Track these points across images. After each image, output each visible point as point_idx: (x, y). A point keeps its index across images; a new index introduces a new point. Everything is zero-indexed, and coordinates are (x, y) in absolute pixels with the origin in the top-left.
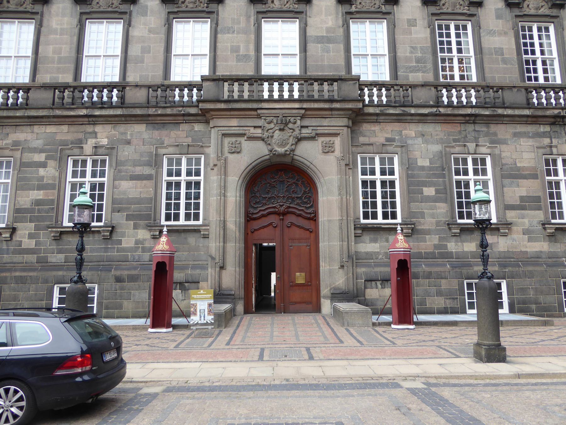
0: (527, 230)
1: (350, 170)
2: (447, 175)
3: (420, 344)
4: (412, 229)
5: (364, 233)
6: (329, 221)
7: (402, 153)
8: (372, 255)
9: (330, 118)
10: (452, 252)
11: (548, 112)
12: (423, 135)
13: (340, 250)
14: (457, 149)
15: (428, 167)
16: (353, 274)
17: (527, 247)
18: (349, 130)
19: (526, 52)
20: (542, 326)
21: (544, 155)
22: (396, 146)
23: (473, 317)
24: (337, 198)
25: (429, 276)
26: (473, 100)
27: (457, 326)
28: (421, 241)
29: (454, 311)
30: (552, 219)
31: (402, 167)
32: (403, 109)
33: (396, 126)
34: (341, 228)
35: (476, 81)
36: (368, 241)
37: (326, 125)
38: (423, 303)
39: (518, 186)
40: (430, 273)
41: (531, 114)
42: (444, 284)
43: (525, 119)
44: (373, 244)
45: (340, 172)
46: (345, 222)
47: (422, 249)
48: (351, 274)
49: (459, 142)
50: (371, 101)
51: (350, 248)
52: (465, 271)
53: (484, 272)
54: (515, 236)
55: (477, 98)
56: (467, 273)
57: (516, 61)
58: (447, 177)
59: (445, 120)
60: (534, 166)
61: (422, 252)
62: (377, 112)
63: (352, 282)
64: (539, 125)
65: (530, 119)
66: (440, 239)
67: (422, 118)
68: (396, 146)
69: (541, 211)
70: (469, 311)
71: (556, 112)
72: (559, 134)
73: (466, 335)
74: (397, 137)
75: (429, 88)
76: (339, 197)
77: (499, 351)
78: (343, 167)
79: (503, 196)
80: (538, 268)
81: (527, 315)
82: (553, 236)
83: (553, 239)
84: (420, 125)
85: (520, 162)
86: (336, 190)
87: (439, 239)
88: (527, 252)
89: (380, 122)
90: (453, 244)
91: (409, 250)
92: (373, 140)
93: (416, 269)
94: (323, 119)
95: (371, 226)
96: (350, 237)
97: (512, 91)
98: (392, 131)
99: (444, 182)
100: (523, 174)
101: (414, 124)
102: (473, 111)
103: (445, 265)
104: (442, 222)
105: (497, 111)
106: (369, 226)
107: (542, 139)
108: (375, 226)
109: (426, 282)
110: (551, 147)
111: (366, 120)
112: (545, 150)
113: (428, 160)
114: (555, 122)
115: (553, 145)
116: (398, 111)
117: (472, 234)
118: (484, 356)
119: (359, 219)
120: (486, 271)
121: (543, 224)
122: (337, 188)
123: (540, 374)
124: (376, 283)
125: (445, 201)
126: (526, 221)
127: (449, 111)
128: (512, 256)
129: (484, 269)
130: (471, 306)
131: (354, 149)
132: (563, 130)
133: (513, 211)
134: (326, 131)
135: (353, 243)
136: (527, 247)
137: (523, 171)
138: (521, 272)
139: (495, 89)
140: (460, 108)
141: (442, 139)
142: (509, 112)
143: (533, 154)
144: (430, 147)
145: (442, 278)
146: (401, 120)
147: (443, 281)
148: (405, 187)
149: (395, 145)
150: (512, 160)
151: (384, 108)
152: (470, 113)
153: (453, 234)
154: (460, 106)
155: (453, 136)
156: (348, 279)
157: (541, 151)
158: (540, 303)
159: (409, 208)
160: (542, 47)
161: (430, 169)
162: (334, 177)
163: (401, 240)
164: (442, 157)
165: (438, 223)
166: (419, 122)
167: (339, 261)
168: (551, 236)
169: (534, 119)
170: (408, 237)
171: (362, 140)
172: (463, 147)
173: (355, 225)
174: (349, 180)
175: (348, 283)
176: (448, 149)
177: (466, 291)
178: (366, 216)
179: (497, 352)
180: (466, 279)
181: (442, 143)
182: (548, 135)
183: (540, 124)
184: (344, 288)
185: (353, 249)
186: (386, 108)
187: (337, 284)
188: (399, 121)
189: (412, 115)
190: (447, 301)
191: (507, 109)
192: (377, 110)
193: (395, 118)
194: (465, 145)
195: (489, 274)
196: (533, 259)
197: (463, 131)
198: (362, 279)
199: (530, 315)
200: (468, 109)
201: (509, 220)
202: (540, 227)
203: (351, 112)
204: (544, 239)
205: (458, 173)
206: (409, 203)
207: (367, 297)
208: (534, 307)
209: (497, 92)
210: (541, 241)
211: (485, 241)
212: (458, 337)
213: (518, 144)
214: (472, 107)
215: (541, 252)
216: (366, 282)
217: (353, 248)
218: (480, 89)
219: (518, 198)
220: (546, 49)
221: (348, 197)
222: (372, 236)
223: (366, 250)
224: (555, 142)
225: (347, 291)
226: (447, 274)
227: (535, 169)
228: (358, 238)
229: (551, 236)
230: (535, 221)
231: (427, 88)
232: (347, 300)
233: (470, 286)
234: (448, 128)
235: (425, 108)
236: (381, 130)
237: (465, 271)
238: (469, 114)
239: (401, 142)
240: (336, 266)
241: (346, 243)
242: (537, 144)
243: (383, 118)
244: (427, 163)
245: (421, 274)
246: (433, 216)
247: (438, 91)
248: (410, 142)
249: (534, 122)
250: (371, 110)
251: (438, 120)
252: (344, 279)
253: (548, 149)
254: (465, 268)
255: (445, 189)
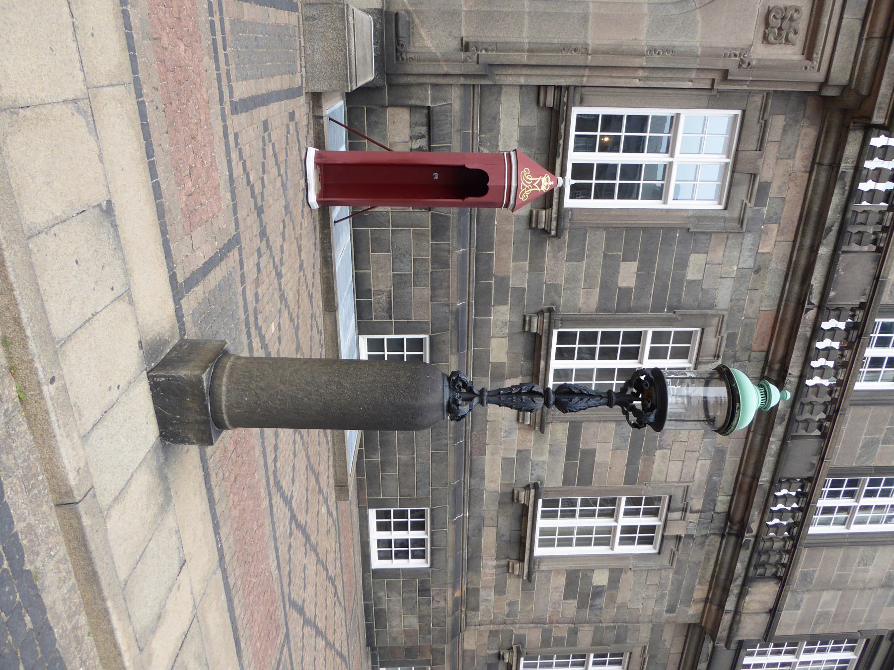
0: (528, 458)
1: (709, 82)
2: (658, 315)
3: (244, 193)
4: (546, 232)
5: (545, 114)
6: (585, 19)
7: (725, 220)
8: (491, 131)
9: (861, 34)
10: (489, 313)
11: (756, 513)
12: (757, 271)
13: (507, 43)
14: (711, 341)
15: (684, 275)
16: (446, 75)
17: (493, 454)
18: (813, 88)
19: (873, 483)
20: (336, 480)
21: (670, 497)
22: (744, 208)
23: (351, 348)
24: (644, 43)
25: (440, 260)
26: (815, 380)
27: (325, 310)
28: (516, 249)
29: (362, 310)
30: (544, 501)
31: (693, 217)
32: (835, 228)
33: (791, 212)
34: (564, 48)
35: (855, 388)
36: (525, 122)
37: (844, 21)
38: (379, 244)
39: (615, 449)
40: (446, 265)
41: (760, 483)
42: (421, 293)
43: (750, 471)
44: (516, 135)
45: (711, 53)
46: (579, 60)
47: (498, 251)
48: (445, 69)
49: (727, 346)
50: (873, 153)
51: (511, 71)
52: (448, 337)
53: (470, 390)
54: (516, 436)
55: (815, 389)
56: (444, 342)
57: (864, 465)
58: (654, 315)
59: (782, 321)
60: (652, 478)
61: (492, 249)
62: (843, 165)
63: (426, 72)
64: (731, 493)
65: (748, 480)
66: (519, 291)
67: (800, 272)
68: (744, 208)
69: (561, 484)
70: (363, 340)
71: (754, 526)
72: (705, 526)
73: (297, 329)
74: (765, 210)
75: (867, 292)
76: (646, 49)
77: (197, 422)
78: (721, 65)
79: (600, 422)
80: (451, 471)
81: (361, 446)
82: (513, 500)
83: (507, 499)
84: (783, 267)
85: (663, 457)
86: (661, 40)
87: (519, 289)
88: (484, 454)
89: (810, 173)
90: (508, 317)
91: (512, 202)
92: (771, 150)
93: (455, 235)
94: (863, 12)
95: (562, 131)
96: (538, 72)
97: (815, 455)
98: (783, 199)
99: (645, 309)
100: (638, 459)
101: (788, 253)
102: (792, 379)
103: (461, 299)
104: (556, 298)
105: (780, 424)
106: (563, 126)
107: (702, 496)
108: (561, 142)
109: (425, 253)
110: (684, 510)
111: (826, 137)
112: (680, 500)
113: (698, 277)
114: (731, 522)
115: (688, 514)
116: (833, 215)
117: (525, 356)
118: (173, 373)
119: (581, 103)
120: (476, 400)
121: (536, 486)
122: (668, 43)
123: (95, 574)
124: (423, 137)
125: (601, 308)
126: (545, 457)
127: (804, 330)
128: (477, 427)
129: (482, 391)
130: (375, 345)
131: (758, 100)
132: (712, 532)
133: (566, 437)
134: (825, 21)
135: (522, 81)
136: (493, 454)
137: (644, 460)
138: (445, 442)
139: (827, 424)
140: (804, 354)
141: (741, 310)
142: (774, 446)
143: (676, 480)
144: (729, 283)
145: (433, 289)
146: (806, 224)
147: (427, 292)
148: (643, 222)
149: (749, 205)
150: (670, 441)
151: (848, 184)
152: (790, 371)
153: (527, 319)
154: (810, 353)
155: (743, 335)
156: (434, 60)
157: (679, 494)
158: (383, 471)
159: (596, 228)
160: (875, 509)
161: (679, 281)
162: (698, 37)
163: (540, 185)
164: (699, 307)
165: (554, 288)
166: (791, 265)
167: (480, 40)
168: (513, 497)
169: (746, 487)
170: (527, 221)
171: (778, 122)
172: (713, 353)
173: (568, 88)
174: (683, 80)
175: (424, 60)
176: (715, 321)
177: (405, 337)
178: (585, 122)
179: (193, 417)
180: (431, 338)
181: (731, 310)
182: (708, 507)
183: (733, 496)
184: (412, 49)
185: (509, 79)
186: (847, 188)
187: (423, 32)
188: (804, 219)
189: (814, 250)
190: (384, 298)
191: (780, 443)
192: (847, 166)
193: (816, 208)
194: (718, 357)
195: (464, 408)
196: (468, 463)
197: (749, 356)
198: (434, 100)
199: (360, 452)
200: (800, 368)
201: (549, 428)
202: (530, 480)
203: (864, 92)
204: (508, 485)
205: (658, 337)
206: (607, 228)
207: (390, 111)
208: (377, 458)
209: (820, 428)
210: (503, 479)
211: (582, 404)
212: (287, 306)
213: (700, 455)
214: (802, 378)
215: (483, 478)
216: (426, 111)
217: (510, 80)
218: (836, 395)
219: (591, 448)
220: (871, 515)
221: (641, 73)
222: (536, 134)
223: (502, 116)
224: (693, 517)
225: (404, 56)
226: (444, 300)
227: (646, 481)
228: (533, 96)
229: (513, 497)
230: (543, 473)
231: (869, 287)
232: (382, 55)
233: (417, 344)
234: (763, 327)
235: (823, 280)
236: (791, 175)
237: (448, 337)
238: (786, 371)
239: (753, 219)
240: (467, 32)
241: (525, 61)
242: (693, 488)
243: (823, 179)
244: (692, 274)
245: (443, 244)
246: (572, 279)
247: (853, 310)
248: (749, 239)
249: (740, 487)
250: (851, 149)
251: (786, 305)
252: (433, 49)
253: (681, 505)
254: (454, 338)
255: (630, 310)
